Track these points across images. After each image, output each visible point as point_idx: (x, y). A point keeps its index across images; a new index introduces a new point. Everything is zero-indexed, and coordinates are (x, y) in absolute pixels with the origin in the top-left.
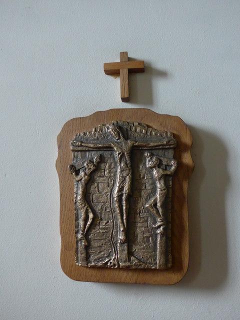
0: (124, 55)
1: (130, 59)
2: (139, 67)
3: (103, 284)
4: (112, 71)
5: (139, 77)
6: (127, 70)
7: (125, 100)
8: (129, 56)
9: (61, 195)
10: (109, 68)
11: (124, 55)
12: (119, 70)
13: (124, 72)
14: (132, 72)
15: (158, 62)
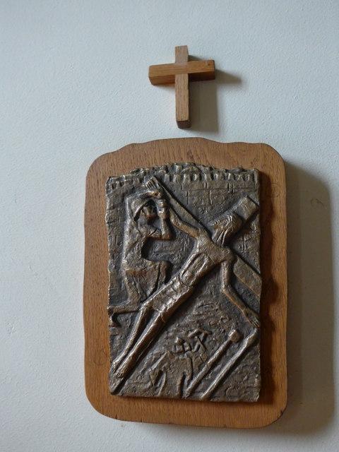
0: (181, 50)
1: (191, 58)
2: (209, 69)
3: (158, 425)
4: (162, 78)
5: (203, 87)
6: (187, 75)
7: (183, 125)
8: (191, 53)
9: (84, 286)
10: (159, 77)
11: (181, 50)
12: (173, 76)
13: (182, 81)
14: (193, 78)
15: (226, 65)
